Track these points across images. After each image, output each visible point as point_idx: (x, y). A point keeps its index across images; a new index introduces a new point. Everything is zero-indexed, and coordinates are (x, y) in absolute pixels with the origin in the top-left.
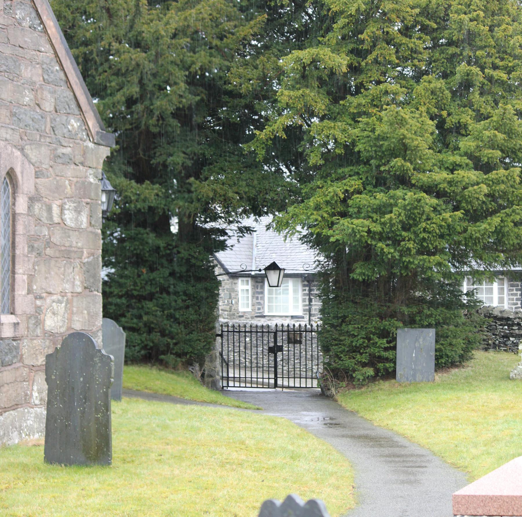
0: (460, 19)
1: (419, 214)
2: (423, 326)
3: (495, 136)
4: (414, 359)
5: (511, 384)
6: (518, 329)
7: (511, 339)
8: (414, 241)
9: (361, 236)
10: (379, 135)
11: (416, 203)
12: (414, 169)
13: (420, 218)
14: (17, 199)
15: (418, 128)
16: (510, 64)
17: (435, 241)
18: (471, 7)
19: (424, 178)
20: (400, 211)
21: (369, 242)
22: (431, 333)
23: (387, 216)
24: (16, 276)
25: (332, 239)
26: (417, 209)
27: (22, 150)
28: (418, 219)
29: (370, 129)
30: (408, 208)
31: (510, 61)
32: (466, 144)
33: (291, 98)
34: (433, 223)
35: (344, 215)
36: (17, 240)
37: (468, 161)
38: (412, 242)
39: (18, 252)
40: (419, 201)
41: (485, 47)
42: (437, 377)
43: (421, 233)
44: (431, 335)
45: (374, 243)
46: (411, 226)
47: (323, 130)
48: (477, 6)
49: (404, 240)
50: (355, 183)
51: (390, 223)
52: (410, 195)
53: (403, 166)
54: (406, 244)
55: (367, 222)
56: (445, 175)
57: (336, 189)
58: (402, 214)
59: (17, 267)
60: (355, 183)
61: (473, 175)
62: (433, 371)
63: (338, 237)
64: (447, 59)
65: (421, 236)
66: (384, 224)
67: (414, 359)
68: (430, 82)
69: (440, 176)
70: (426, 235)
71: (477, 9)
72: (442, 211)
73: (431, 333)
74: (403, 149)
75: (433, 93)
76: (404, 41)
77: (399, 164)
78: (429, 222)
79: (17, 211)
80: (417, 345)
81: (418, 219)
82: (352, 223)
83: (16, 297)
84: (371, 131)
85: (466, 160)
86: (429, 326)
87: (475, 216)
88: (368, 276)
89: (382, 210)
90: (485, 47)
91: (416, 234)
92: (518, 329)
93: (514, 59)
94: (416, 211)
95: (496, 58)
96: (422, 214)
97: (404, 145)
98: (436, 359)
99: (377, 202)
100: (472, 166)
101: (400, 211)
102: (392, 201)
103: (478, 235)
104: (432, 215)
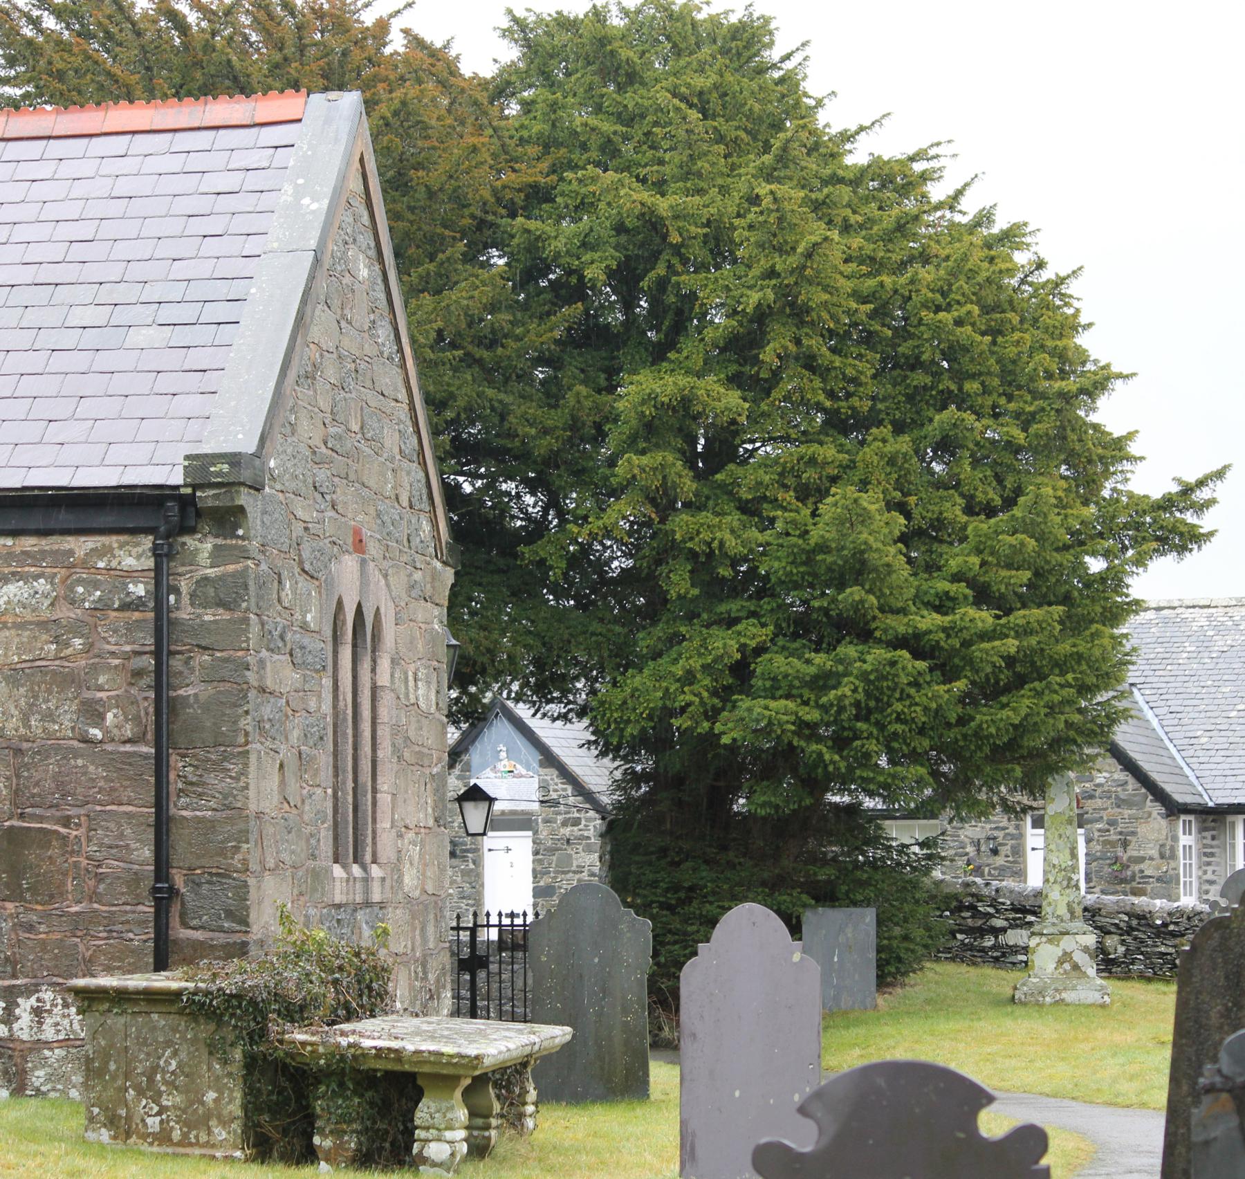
0: (940, 321)
1: (888, 688)
2: (855, 904)
3: (1022, 544)
4: (836, 967)
5: (1019, 1010)
6: (972, 917)
7: (959, 936)
8: (877, 740)
9: (783, 731)
10: (816, 544)
11: (888, 669)
12: (882, 609)
13: (889, 697)
14: (379, 661)
15: (880, 533)
16: (1028, 409)
17: (912, 739)
18: (952, 296)
19: (899, 625)
20: (857, 683)
21: (795, 743)
22: (869, 916)
23: (832, 694)
24: (378, 795)
25: (725, 740)
26: (887, 679)
27: (386, 576)
28: (885, 699)
29: (798, 532)
30: (872, 677)
31: (1026, 402)
32: (958, 558)
33: (645, 471)
34: (917, 704)
35: (747, 690)
36: (379, 733)
37: (968, 591)
38: (874, 741)
39: (380, 754)
40: (893, 663)
41: (980, 374)
42: (880, 1001)
43: (890, 723)
44: (867, 920)
45: (803, 744)
46: (870, 711)
47: (698, 533)
48: (963, 294)
49: (856, 738)
50: (754, 633)
51: (838, 705)
52: (878, 654)
53: (862, 601)
54: (863, 746)
55: (791, 705)
56: (936, 619)
57: (726, 644)
58: (860, 690)
59: (380, 780)
60: (754, 633)
61: (984, 618)
62: (874, 988)
63: (735, 734)
64: (907, 395)
65: (892, 728)
66: (825, 709)
67: (836, 967)
68: (884, 441)
69: (929, 621)
70: (899, 728)
71: (963, 300)
72: (925, 685)
73: (869, 916)
74: (857, 569)
75: (892, 461)
76: (837, 364)
77: (857, 598)
78: (908, 703)
79: (379, 684)
80: (841, 939)
81: (885, 699)
82: (766, 708)
83: (379, 832)
84: (799, 536)
85: (961, 589)
86: (867, 903)
87: (992, 690)
88: (777, 807)
89: (823, 681)
90: (980, 374)
91: (881, 727)
92: (972, 917)
93: (1034, 399)
94: (885, 684)
95: (1000, 395)
96: (894, 690)
97: (863, 563)
98: (878, 967)
99: (812, 670)
100: (971, 599)
101: (857, 683)
102: (841, 668)
103: (993, 730)
104: (912, 691)
